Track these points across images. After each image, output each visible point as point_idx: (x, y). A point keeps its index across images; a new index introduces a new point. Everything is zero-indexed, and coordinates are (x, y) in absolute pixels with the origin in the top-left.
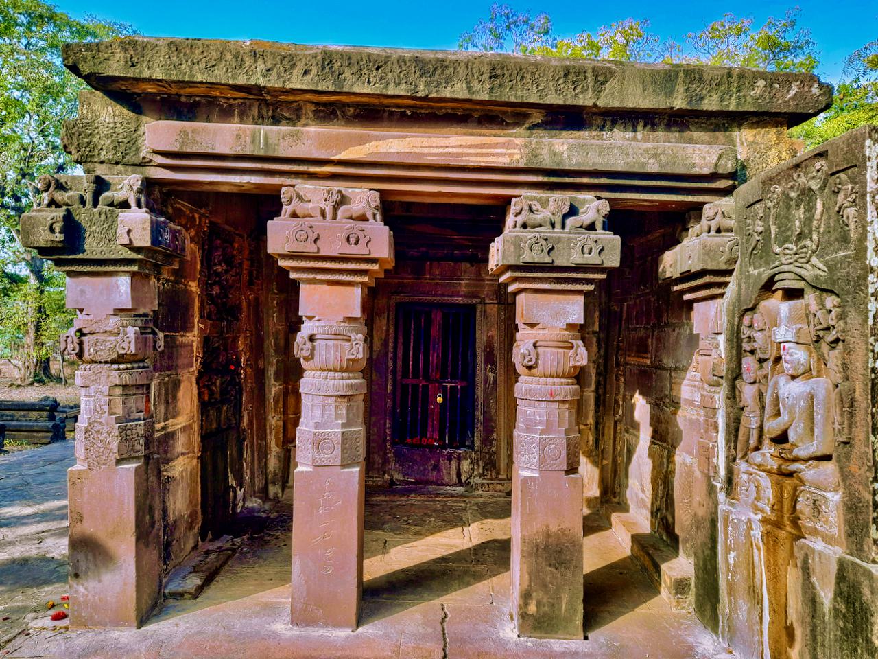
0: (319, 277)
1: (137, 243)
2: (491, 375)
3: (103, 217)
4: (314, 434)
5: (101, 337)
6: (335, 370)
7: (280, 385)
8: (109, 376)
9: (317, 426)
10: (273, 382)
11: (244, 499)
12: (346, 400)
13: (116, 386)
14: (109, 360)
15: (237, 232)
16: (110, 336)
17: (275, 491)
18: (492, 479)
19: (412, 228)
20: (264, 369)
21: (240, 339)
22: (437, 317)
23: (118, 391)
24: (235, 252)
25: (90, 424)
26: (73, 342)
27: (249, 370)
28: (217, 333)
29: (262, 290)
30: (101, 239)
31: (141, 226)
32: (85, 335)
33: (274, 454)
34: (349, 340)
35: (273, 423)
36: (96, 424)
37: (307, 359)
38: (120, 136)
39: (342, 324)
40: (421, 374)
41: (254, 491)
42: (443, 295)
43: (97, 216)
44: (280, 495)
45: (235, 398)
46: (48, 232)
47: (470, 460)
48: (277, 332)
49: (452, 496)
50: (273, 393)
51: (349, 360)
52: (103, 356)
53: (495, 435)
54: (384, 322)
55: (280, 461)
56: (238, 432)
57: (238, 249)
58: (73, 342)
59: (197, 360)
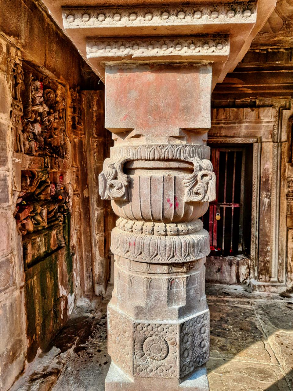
0: (139, 52)
2: (266, 200)
4: (136, 326)
6: (166, 220)
7: (101, 209)
9: (139, 311)
10: (95, 207)
11: (75, 300)
12: (185, 269)
15: (59, 81)
17: (100, 289)
18: (266, 281)
20: (88, 197)
21: (67, 174)
24: (58, 99)
27: (76, 198)
28: (40, 168)
29: (85, 134)
33: (98, 262)
34: (191, 171)
37: (120, 202)
39: (178, 142)
41: (84, 292)
42: (226, 136)
44: (104, 293)
45: (64, 222)
47: (247, 266)
49: (237, 297)
51: (188, 204)
53: (269, 248)
55: (103, 267)
56: (68, 250)
57: (61, 96)
59: (13, 195)
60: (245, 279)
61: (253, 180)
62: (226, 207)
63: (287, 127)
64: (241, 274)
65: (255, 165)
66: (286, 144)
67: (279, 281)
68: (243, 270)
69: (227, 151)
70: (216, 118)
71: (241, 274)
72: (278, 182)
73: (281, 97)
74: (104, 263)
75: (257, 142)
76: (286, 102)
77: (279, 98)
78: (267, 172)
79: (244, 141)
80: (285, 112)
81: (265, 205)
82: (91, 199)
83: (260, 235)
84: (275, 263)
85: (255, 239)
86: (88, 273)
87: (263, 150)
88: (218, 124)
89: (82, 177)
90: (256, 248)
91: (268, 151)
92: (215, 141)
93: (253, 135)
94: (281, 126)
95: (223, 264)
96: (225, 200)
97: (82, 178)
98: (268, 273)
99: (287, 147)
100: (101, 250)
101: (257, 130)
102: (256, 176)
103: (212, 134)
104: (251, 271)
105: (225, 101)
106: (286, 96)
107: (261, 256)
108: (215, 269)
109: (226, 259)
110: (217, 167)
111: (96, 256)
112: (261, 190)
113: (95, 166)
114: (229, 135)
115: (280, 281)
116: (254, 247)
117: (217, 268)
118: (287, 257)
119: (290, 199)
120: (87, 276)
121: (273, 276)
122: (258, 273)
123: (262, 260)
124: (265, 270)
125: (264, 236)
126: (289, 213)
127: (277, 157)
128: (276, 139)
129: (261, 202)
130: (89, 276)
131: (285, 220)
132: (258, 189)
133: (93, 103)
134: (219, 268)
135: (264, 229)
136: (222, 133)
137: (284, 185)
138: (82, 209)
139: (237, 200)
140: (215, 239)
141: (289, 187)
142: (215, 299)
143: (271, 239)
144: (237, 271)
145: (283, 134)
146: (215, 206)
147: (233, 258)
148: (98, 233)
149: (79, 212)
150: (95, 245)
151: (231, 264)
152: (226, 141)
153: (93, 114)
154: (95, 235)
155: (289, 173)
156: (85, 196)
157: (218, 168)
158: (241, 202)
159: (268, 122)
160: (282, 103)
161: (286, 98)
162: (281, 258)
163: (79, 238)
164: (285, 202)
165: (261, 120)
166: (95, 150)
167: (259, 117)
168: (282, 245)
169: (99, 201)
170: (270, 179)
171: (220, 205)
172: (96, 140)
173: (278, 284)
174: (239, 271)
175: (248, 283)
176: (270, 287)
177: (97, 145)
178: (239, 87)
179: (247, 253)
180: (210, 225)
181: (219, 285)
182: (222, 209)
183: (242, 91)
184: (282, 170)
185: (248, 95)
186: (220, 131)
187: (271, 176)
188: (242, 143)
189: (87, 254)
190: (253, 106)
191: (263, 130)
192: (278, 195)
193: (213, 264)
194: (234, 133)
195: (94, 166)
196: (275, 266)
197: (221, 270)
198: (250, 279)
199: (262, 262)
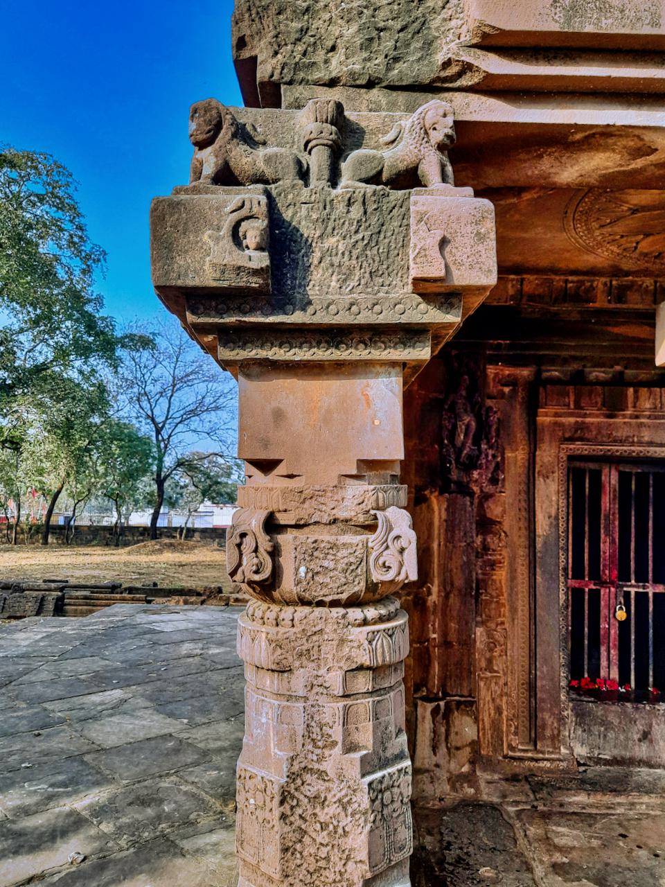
1: (461, 278)
3: (356, 212)
5: (325, 536)
8: (342, 641)
13: (361, 668)
14: (344, 596)
16: (344, 532)
19: (616, 330)
22: (611, 479)
23: (363, 683)
25: (292, 777)
26: (256, 550)
30: (351, 270)
31: (474, 228)
32: (282, 528)
36: (308, 777)
38: (382, 14)
40: (586, 572)
42: (651, 444)
43: (341, 208)
46: (227, 243)
52: (329, 587)
58: (256, 550)
62: (636, 593)
69: (634, 471)
70: (634, 407)
88: (637, 417)
92: (625, 451)
95: (654, 723)
96: (633, 576)
108: (637, 733)
109: (659, 710)
110: (614, 504)
134: (644, 732)
136: (643, 437)
140: (615, 664)
142: (659, 802)
146: (613, 589)
152: (648, 452)
157: (617, 506)
171: (623, 586)
180: (602, 632)
181: (644, 770)
182: (627, 594)
186: (639, 432)
197: (649, 736)
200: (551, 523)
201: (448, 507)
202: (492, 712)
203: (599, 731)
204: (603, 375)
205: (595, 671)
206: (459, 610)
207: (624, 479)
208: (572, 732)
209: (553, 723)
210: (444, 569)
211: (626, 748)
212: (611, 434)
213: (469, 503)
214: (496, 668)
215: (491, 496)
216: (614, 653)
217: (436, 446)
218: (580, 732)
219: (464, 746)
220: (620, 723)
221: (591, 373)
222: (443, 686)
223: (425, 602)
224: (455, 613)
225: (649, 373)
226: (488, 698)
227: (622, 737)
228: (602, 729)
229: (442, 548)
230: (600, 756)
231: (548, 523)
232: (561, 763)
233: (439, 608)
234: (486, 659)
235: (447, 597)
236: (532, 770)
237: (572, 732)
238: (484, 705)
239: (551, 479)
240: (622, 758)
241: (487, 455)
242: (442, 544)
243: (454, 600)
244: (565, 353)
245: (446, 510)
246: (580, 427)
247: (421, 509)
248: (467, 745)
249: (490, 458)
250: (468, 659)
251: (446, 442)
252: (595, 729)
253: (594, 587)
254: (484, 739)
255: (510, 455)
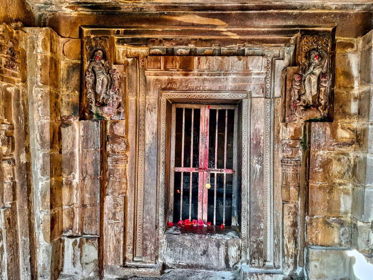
7: (47, 179)
18: (259, 267)
19: (179, 19)
22: (205, 114)
35: (41, 217)
47: (237, 247)
48: (42, 127)
50: (40, 187)
53: (262, 226)
54: (155, 116)
55: (48, 255)
60: (235, 264)
61: (243, 142)
63: (280, 80)
64: (231, 257)
65: (245, 125)
66: (279, 100)
67: (275, 266)
68: (233, 252)
69: (218, 109)
71: (231, 257)
72: (272, 145)
73: (273, 45)
74: (50, 249)
75: (247, 98)
76: (279, 51)
77: (271, 47)
78: (257, 133)
79: (232, 97)
80: (278, 62)
81: (257, 173)
82: (34, 165)
83: (251, 209)
84: (271, 243)
85: (246, 213)
86: (25, 265)
87: (252, 107)
88: (201, 75)
89: (18, 137)
90: (248, 224)
91: (259, 109)
93: (241, 89)
94: (274, 79)
97: (19, 139)
98: (262, 257)
99: (280, 104)
100: (46, 233)
101: (246, 84)
102: (246, 138)
103: (193, 87)
104: (242, 253)
105: (209, 49)
106: (278, 43)
107: (253, 235)
109: (213, 238)
111: (40, 240)
112: (251, 155)
113: (39, 123)
114: (214, 89)
115: (276, 266)
116: (246, 223)
117: (203, 250)
118: (283, 237)
119: (286, 165)
120: (24, 269)
121: (268, 259)
122: (250, 256)
123: (255, 240)
124: (258, 253)
125: (256, 210)
126: (284, 183)
127: (271, 115)
128: (269, 94)
129: (252, 169)
130: (27, 268)
131: (280, 191)
132: (249, 153)
133: (37, 43)
135: (256, 202)
137: (278, 148)
138: (18, 179)
139: (229, 167)
141: (283, 151)
143: (265, 214)
144: (225, 254)
145: (276, 88)
147: (221, 237)
148: (42, 211)
149: (10, 184)
150: (39, 227)
151: (218, 245)
153: (37, 57)
154: (39, 213)
155: (284, 135)
156: (22, 162)
158: (233, 168)
159: (259, 74)
160: (275, 53)
161: (278, 47)
162: (276, 238)
163: (9, 219)
164: (280, 169)
165: (250, 71)
166: (40, 102)
167: (247, 68)
168: (278, 222)
169: (44, 168)
170: (262, 141)
171: (210, 171)
172: (41, 90)
173: (274, 270)
174: (229, 253)
175: (239, 268)
176: (263, 275)
177: (42, 96)
178: (223, 32)
179: (238, 230)
183: (226, 35)
184: (276, 131)
185: (235, 41)
186: (204, 84)
187: (262, 138)
188: (230, 98)
189: (24, 239)
190: (241, 54)
191: (253, 83)
192: (272, 161)
193: (197, 246)
194: (220, 87)
195: (37, 123)
196: (270, 247)
197: (207, 253)
198: (242, 263)
199: (254, 242)
200: (154, 137)
201: (84, 128)
202: (115, 242)
203: (180, 251)
204: (184, 50)
205: (195, 217)
206: (91, 187)
207: (212, 113)
208: (165, 251)
209: (151, 247)
210: (82, 163)
211: (194, 259)
212: (188, 85)
213: (96, 126)
214: (117, 218)
215: (117, 122)
216: (205, 206)
217: (76, 92)
218: (169, 251)
219: (90, 263)
220: (191, 245)
221: (177, 49)
222: (81, 229)
223: (71, 183)
224: (88, 189)
225: (211, 49)
226: (113, 234)
227: (192, 253)
228: (181, 249)
229: (81, 152)
230: (180, 263)
231: (152, 137)
232: (151, 270)
233: (79, 186)
234: (112, 213)
235: (84, 179)
236: (135, 273)
237: (165, 251)
238: (110, 238)
239: (154, 112)
240: (192, 265)
241: (113, 98)
242: (80, 149)
243: (88, 181)
244: (159, 36)
245: (83, 130)
246: (171, 82)
247: (68, 129)
248: (92, 262)
249: (115, 99)
250: (95, 214)
251: (90, 90)
252: (178, 249)
253: (195, 172)
254: (110, 256)
255: (132, 98)
